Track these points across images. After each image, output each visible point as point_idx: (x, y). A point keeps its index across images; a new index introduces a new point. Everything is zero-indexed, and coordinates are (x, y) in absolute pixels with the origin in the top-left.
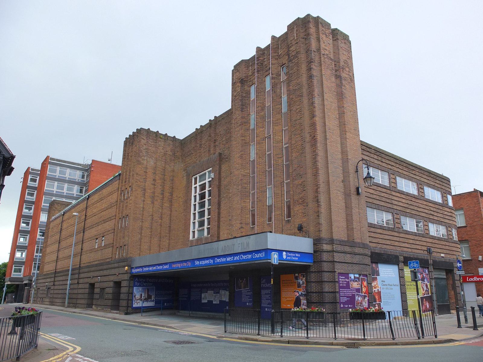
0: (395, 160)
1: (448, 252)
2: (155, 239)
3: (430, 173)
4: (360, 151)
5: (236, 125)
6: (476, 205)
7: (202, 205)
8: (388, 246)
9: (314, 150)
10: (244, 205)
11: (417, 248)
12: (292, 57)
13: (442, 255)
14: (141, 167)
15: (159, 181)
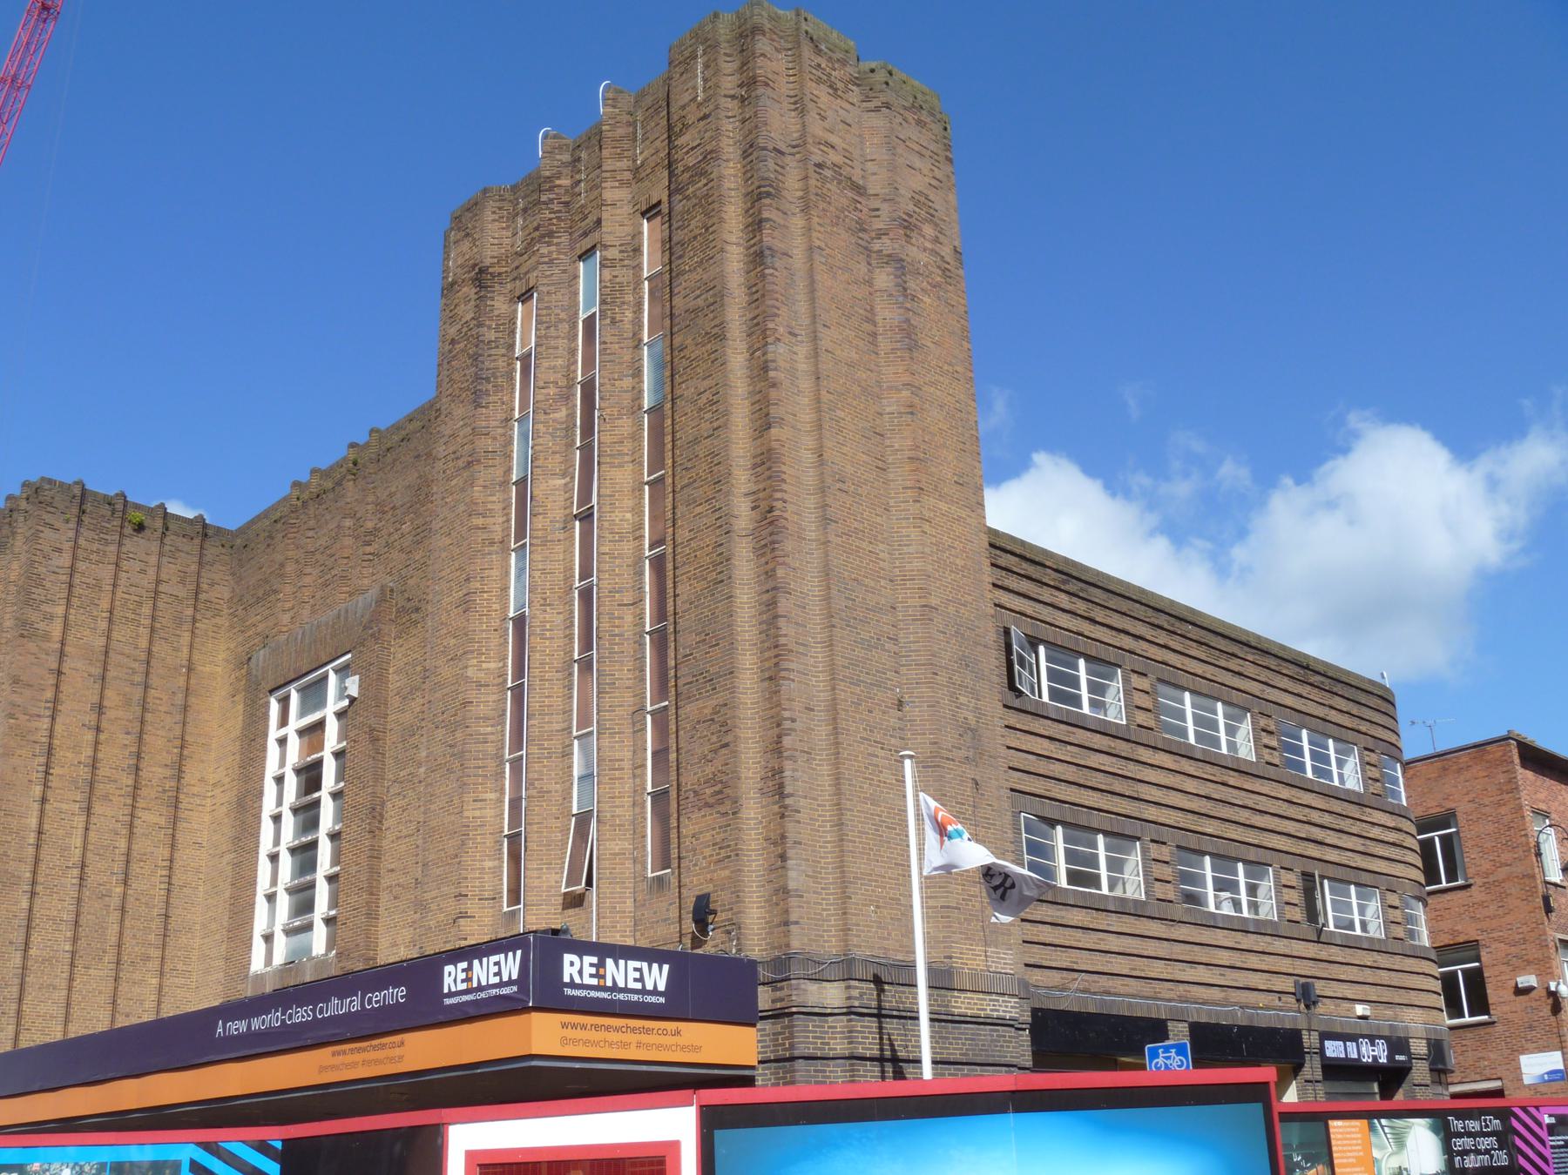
0: (1150, 612)
1: (1387, 995)
2: (91, 971)
3: (1307, 668)
4: (988, 575)
5: (451, 464)
6: (1506, 797)
7: (307, 813)
8: (1119, 981)
9: (771, 566)
10: (477, 813)
11: (1252, 985)
12: (686, 175)
13: (1360, 1009)
14: (35, 650)
15: (120, 713)
